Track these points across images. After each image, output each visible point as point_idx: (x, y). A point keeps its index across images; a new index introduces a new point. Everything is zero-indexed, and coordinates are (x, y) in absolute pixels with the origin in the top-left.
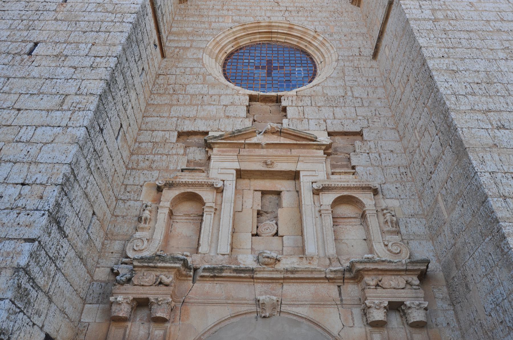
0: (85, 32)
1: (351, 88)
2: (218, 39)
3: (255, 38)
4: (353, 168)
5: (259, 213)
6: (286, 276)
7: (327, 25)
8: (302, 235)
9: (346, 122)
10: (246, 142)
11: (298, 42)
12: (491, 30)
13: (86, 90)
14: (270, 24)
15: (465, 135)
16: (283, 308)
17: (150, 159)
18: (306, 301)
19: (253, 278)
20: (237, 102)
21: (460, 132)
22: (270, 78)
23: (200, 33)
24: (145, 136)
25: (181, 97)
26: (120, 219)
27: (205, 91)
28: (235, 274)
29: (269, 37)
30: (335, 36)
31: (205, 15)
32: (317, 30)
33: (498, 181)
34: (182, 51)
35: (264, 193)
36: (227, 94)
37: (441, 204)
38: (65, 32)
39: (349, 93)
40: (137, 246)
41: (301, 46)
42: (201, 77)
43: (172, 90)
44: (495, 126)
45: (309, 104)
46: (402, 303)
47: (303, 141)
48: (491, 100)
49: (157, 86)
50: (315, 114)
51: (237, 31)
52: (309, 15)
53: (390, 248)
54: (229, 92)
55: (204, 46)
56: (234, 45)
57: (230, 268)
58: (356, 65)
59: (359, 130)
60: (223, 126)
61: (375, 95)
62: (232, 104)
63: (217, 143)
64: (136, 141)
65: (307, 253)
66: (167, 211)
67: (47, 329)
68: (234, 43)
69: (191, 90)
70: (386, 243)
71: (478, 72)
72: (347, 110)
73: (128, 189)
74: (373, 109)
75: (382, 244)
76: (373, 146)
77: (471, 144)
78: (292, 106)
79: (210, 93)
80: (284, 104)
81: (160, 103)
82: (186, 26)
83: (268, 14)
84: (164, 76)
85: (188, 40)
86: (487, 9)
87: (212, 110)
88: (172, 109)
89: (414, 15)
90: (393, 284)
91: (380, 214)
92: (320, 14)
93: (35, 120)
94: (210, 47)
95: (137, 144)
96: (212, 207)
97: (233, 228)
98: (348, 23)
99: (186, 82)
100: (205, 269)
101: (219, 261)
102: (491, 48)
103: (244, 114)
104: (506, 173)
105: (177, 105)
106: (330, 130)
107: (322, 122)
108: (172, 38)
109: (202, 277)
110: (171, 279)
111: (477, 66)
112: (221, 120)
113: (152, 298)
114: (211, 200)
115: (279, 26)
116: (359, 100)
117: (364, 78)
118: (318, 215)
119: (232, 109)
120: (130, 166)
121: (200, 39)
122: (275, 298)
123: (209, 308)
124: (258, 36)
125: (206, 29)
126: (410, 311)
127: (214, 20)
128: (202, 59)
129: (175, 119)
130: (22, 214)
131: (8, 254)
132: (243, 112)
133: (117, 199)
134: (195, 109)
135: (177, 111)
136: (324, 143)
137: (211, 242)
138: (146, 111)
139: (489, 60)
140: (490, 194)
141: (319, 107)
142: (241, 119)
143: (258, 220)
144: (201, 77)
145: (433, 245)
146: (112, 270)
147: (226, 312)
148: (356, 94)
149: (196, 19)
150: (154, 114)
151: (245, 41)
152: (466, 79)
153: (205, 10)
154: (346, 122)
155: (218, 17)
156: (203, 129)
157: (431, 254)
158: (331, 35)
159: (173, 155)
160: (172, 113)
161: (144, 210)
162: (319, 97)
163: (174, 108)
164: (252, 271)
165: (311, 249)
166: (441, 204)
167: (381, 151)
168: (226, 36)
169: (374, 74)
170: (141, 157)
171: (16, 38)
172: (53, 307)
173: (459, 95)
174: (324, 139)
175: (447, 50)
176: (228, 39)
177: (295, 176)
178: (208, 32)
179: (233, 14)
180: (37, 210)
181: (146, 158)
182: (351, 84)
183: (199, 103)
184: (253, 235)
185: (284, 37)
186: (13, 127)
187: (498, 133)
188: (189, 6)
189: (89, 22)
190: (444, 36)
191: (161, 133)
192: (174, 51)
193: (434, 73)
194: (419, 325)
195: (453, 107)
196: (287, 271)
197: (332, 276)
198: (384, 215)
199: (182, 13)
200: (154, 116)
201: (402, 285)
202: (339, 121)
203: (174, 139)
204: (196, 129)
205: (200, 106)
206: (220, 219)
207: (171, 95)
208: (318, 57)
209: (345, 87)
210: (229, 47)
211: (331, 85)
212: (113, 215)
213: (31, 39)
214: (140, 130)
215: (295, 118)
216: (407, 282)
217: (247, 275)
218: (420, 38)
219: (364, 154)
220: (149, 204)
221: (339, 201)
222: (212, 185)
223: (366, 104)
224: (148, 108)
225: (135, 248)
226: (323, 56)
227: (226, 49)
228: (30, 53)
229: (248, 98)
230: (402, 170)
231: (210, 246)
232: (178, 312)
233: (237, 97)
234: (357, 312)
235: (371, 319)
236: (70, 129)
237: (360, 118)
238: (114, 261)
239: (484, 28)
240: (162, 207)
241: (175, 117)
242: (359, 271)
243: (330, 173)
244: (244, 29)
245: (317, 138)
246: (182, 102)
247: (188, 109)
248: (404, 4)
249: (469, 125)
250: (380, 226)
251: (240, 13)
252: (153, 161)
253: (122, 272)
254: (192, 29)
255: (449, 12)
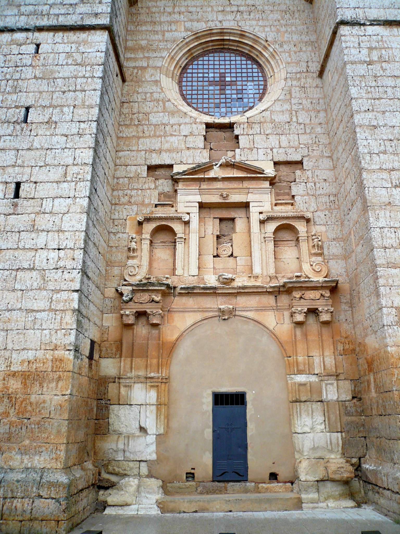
0: (64, 92)
1: (296, 112)
4: (293, 196)
5: (218, 237)
6: (239, 291)
7: (278, 31)
8: (251, 256)
9: (290, 151)
10: (206, 176)
11: (249, 51)
13: (80, 159)
14: (222, 31)
15: (369, 194)
16: (237, 313)
17: (128, 194)
19: (215, 293)
20: (195, 131)
21: (367, 192)
23: (154, 47)
24: (121, 172)
26: (114, 249)
27: (165, 120)
28: (203, 291)
29: (221, 45)
30: (285, 46)
31: (158, 22)
32: (269, 39)
33: (384, 235)
34: (140, 71)
35: (221, 220)
37: (352, 237)
38: (48, 94)
39: (294, 119)
41: (252, 54)
43: (137, 120)
44: (394, 184)
45: (259, 132)
46: (317, 309)
47: (253, 174)
50: (263, 143)
51: (189, 41)
53: (314, 268)
55: (159, 64)
56: (188, 57)
57: (199, 288)
60: (185, 159)
61: (317, 119)
63: (181, 179)
64: (114, 177)
65: (254, 273)
66: (148, 242)
67: (91, 337)
68: (186, 56)
70: (312, 263)
71: (394, 127)
72: (291, 137)
73: (116, 223)
74: (314, 136)
75: (309, 264)
76: (310, 176)
77: (373, 203)
78: (243, 135)
79: (171, 123)
80: (236, 132)
83: (220, 17)
84: (128, 104)
87: (174, 141)
89: (352, 56)
90: (312, 297)
91: (310, 239)
93: (50, 193)
94: (166, 65)
96: (182, 238)
97: (199, 252)
99: (148, 110)
100: (182, 288)
101: (190, 282)
106: (276, 160)
107: (269, 151)
108: (129, 55)
109: (179, 293)
112: (183, 152)
113: (148, 311)
115: (230, 33)
116: (302, 126)
117: (309, 100)
118: (263, 240)
119: (191, 140)
120: (113, 202)
121: (155, 55)
122: (231, 307)
123: (187, 314)
124: (211, 44)
125: (160, 41)
130: (65, 273)
131: (66, 300)
132: (200, 142)
133: (109, 233)
134: (159, 141)
135: (145, 143)
136: (270, 175)
138: (118, 145)
140: (376, 245)
141: (267, 135)
142: (200, 151)
145: (346, 264)
146: (117, 290)
147: (199, 316)
148: (301, 121)
149: (150, 28)
150: (125, 148)
152: (382, 135)
153: (157, 15)
154: (290, 151)
155: (170, 23)
156: (168, 162)
158: (281, 46)
160: (140, 146)
162: (268, 124)
163: (141, 140)
164: (215, 288)
165: (257, 270)
166: (352, 237)
167: (317, 180)
168: (180, 48)
170: (121, 193)
171: (9, 103)
172: (91, 323)
173: (374, 153)
174: (270, 171)
175: (373, 101)
176: (181, 51)
177: (246, 206)
178: (162, 45)
180: (74, 269)
182: (296, 107)
183: (162, 134)
184: (214, 257)
186: (36, 200)
188: (140, 9)
189: (64, 78)
191: (133, 168)
192: (133, 73)
193: (358, 130)
194: (326, 323)
195: (366, 166)
196: (240, 288)
198: (313, 240)
199: (134, 20)
200: (125, 151)
202: (283, 150)
203: (145, 174)
204: (162, 163)
205: (163, 138)
207: (137, 126)
208: (269, 70)
209: (291, 112)
212: (108, 246)
213: (22, 104)
214: (116, 165)
215: (246, 148)
217: (211, 292)
218: (353, 87)
219: (302, 184)
221: (278, 229)
222: (180, 219)
223: (308, 131)
225: (130, 274)
226: (273, 70)
227: (180, 63)
228: (25, 121)
229: (204, 126)
230: (332, 198)
231: (183, 269)
232: (166, 318)
234: (287, 314)
236: (78, 199)
237: (302, 146)
238: (117, 282)
240: (144, 239)
243: (274, 204)
244: (197, 38)
245: (264, 171)
246: (147, 133)
249: (375, 184)
251: (192, 18)
252: (131, 197)
253: (125, 293)
254: (146, 42)
255: (383, 51)
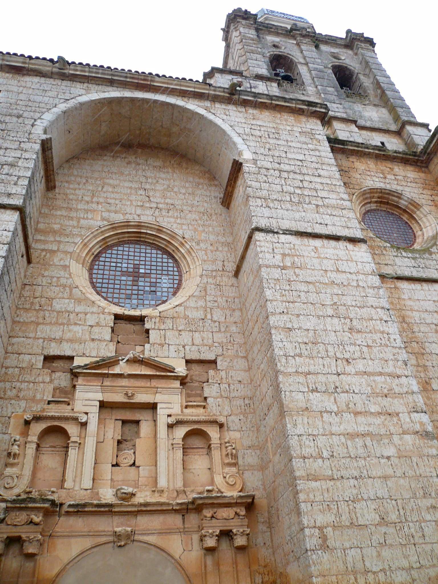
1: (211, 309)
2: (86, 241)
3: (123, 238)
4: (206, 398)
5: (119, 442)
6: (140, 509)
8: (156, 466)
9: (203, 349)
11: (166, 246)
12: (327, 282)
14: (140, 224)
16: (136, 537)
17: (17, 387)
18: (155, 530)
19: (111, 511)
21: (283, 396)
22: (135, 288)
25: (47, 314)
27: (70, 308)
28: (96, 509)
29: (137, 237)
30: (201, 245)
31: (74, 208)
32: (186, 236)
34: (48, 254)
35: (124, 422)
36: (92, 313)
37: (269, 445)
39: (209, 316)
40: (8, 484)
42: (67, 289)
43: (38, 305)
44: (311, 388)
45: (171, 327)
46: (231, 531)
47: (162, 372)
48: (312, 362)
49: (23, 299)
50: (175, 339)
52: (179, 216)
54: (95, 309)
55: (71, 250)
56: (102, 245)
58: (218, 283)
59: (213, 358)
60: (88, 351)
61: (232, 318)
62: (98, 324)
63: (82, 373)
65: (158, 486)
66: (34, 446)
68: (101, 244)
69: (57, 305)
70: (225, 475)
72: (205, 335)
76: (224, 376)
77: (290, 408)
78: (154, 329)
80: (147, 326)
81: (26, 321)
82: (53, 221)
83: (139, 212)
84: (30, 287)
85: (55, 241)
86: (327, 256)
88: (38, 329)
90: (225, 515)
91: (223, 447)
92: (190, 215)
94: (78, 251)
95: (4, 369)
96: (76, 442)
97: (96, 459)
98: (216, 229)
99: (53, 295)
100: (70, 506)
102: (323, 303)
103: (108, 336)
104: (309, 435)
105: (43, 324)
106: (188, 358)
107: (181, 348)
108: (39, 237)
110: (41, 518)
111: (308, 324)
112: (87, 343)
113: (24, 536)
114: (75, 434)
115: (148, 227)
116: (217, 324)
117: (224, 298)
121: (67, 240)
123: (73, 540)
124: (127, 235)
125: (74, 227)
126: (235, 537)
127: (82, 216)
128: (69, 267)
129: (41, 341)
132: (107, 334)
134: (61, 330)
136: (181, 374)
137: (75, 477)
138: (12, 330)
139: (319, 317)
140: (295, 455)
141: (180, 331)
143: (118, 448)
144: (67, 289)
145: (263, 475)
148: (215, 318)
150: (20, 334)
151: (113, 240)
153: (74, 202)
155: (87, 211)
157: (260, 483)
158: (198, 244)
159: (39, 383)
160: (39, 333)
161: (13, 444)
163: (40, 327)
164: (111, 505)
165: (162, 483)
166: (269, 445)
167: (231, 382)
168: (94, 236)
169: (233, 294)
173: (290, 356)
174: (181, 369)
177: (153, 407)
178: (75, 231)
179: (103, 210)
181: (13, 386)
183: (65, 321)
184: (113, 466)
185: (153, 238)
187: (312, 396)
190: (288, 288)
191: (27, 358)
194: (241, 549)
195: (282, 369)
196: (141, 505)
197: (178, 508)
198: (226, 447)
200: (20, 337)
201: (232, 515)
203: (40, 365)
204: (62, 354)
205: (66, 326)
206: (84, 453)
207: (37, 311)
209: (205, 309)
210: (96, 248)
211: (192, 305)
214: (6, 353)
215: (157, 343)
216: (236, 513)
217: (106, 510)
220: (18, 437)
221: (188, 435)
223: (223, 329)
224: (14, 326)
225: (7, 486)
227: (93, 250)
229: (113, 317)
230: (247, 401)
231: (74, 481)
232: (46, 545)
233: (102, 316)
234: (196, 537)
235: (205, 546)
237: (216, 344)
239: (322, 279)
240: (30, 442)
241: (41, 338)
242: (199, 505)
244: (113, 228)
245: (174, 369)
246: (48, 320)
247: (54, 328)
248: (260, 246)
249: (291, 388)
250: (222, 459)
251: (110, 209)
252: (20, 390)
254: (59, 226)
